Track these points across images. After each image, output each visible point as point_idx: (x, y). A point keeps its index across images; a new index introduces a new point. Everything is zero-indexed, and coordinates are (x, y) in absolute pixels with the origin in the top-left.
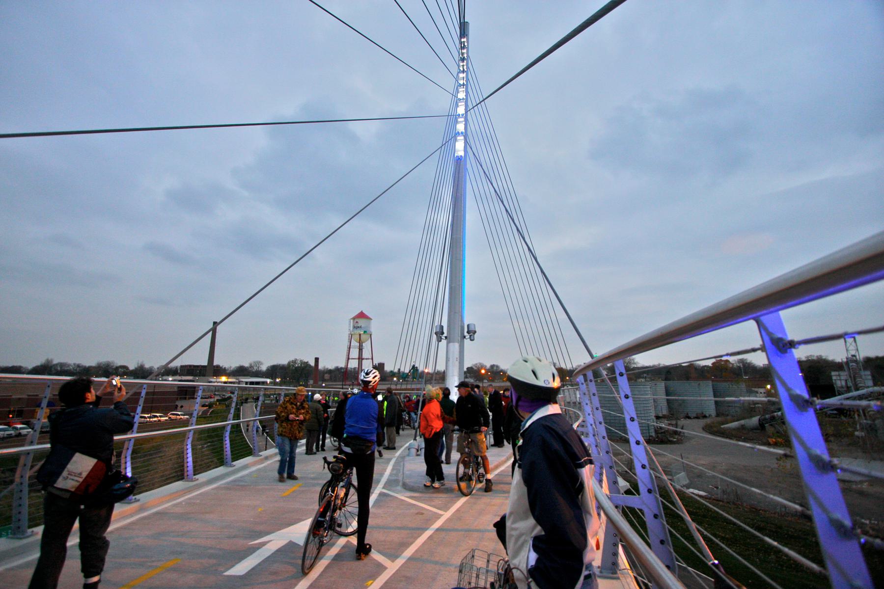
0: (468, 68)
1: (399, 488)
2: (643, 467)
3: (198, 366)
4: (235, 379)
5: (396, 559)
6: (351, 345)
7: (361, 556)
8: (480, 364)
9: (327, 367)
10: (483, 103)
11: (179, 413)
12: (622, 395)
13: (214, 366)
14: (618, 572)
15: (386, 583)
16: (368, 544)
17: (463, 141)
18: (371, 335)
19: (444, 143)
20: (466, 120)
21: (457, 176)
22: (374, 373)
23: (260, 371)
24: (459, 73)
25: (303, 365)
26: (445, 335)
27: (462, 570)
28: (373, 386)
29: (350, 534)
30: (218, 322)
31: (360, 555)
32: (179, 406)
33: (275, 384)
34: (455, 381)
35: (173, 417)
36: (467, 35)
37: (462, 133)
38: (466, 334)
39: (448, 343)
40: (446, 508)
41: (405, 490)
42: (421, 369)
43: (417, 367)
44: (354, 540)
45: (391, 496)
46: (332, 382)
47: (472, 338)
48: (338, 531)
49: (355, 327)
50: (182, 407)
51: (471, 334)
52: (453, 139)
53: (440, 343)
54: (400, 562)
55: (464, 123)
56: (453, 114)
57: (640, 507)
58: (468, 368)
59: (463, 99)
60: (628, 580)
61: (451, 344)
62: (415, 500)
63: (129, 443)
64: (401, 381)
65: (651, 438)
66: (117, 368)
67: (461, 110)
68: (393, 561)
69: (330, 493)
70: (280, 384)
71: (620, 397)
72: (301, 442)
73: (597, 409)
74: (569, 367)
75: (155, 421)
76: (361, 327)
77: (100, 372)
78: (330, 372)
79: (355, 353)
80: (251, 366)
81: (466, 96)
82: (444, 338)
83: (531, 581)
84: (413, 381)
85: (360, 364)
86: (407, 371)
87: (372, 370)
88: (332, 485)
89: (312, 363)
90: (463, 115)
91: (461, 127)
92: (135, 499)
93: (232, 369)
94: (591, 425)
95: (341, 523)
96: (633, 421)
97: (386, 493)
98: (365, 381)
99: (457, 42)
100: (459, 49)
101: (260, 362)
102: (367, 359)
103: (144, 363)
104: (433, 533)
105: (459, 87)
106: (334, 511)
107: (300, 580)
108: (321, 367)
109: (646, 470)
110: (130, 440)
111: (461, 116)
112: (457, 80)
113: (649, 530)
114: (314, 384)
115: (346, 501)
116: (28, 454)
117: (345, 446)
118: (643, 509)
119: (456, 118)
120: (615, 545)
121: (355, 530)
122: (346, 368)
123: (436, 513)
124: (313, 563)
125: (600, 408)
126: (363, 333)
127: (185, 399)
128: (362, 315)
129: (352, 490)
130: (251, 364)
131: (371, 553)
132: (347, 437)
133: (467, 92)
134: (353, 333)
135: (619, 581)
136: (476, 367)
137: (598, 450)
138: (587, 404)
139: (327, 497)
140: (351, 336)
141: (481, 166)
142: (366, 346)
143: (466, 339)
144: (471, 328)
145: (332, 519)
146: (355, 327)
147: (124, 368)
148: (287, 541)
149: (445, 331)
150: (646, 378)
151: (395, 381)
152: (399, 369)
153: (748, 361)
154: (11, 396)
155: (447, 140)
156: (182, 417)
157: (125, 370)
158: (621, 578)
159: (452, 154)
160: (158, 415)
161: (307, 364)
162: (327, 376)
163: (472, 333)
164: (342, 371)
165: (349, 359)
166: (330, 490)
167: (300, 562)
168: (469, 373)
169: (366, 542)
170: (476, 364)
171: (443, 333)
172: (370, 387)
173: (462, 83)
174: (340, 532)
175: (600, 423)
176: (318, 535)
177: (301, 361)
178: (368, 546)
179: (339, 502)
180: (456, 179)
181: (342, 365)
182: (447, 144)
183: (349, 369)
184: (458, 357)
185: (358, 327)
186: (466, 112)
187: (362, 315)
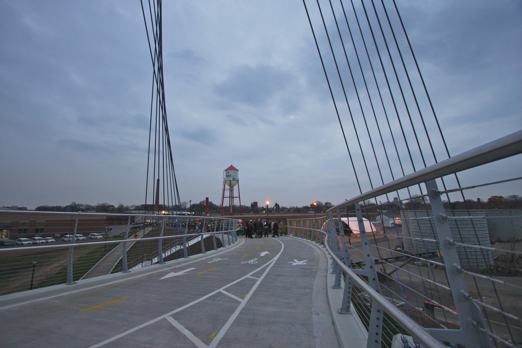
6: (225, 188)
13: (159, 205)
18: (238, 181)
30: (158, 179)
43: (278, 205)
53: (158, 179)
76: (231, 176)
101: (186, 202)
116: (185, 237)
126: (232, 179)
127: (121, 224)
128: (232, 168)
140: (225, 182)
142: (236, 188)
154: (19, 221)
185: (229, 176)
187: (232, 168)
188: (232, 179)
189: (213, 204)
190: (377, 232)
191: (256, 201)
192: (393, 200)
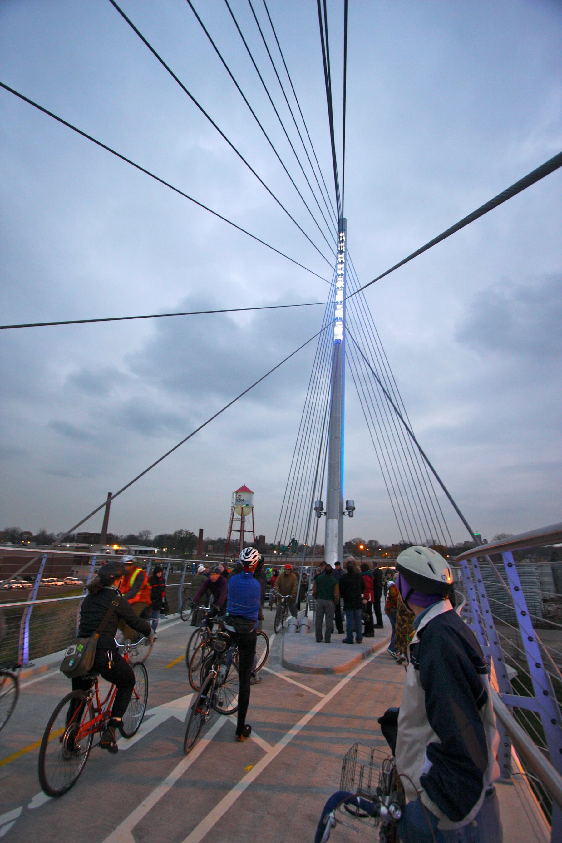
0: (346, 259)
1: (279, 666)
2: (538, 665)
3: (92, 534)
4: (125, 547)
5: (276, 744)
7: (240, 738)
8: (359, 539)
9: (210, 538)
10: (360, 292)
11: (74, 578)
12: (512, 587)
13: (107, 535)
14: (512, 776)
15: (266, 769)
16: (248, 725)
17: (342, 326)
18: (252, 508)
19: (324, 328)
20: (344, 307)
21: (336, 358)
22: (253, 553)
23: (149, 540)
24: (337, 264)
25: (188, 536)
26: (324, 511)
27: (345, 766)
28: (253, 566)
29: (229, 712)
31: (239, 737)
32: (75, 571)
33: (161, 553)
34: (334, 557)
35: (68, 582)
36: (345, 230)
37: (340, 318)
38: (345, 510)
39: (327, 519)
40: (326, 691)
41: (285, 669)
42: (301, 542)
44: (234, 719)
45: (271, 674)
46: (214, 552)
47: (351, 515)
48: (219, 709)
49: (238, 500)
50: (77, 572)
51: (350, 510)
52: (331, 324)
53: (319, 518)
54: (280, 746)
55: (342, 309)
56: (331, 302)
57: (536, 710)
58: (346, 543)
59: (342, 288)
60: (522, 787)
61: (330, 520)
62: (295, 680)
63: (28, 610)
64: (281, 554)
65: (538, 622)
66: (22, 534)
67: (340, 297)
68: (273, 746)
69: (213, 670)
70: (167, 554)
71: (509, 588)
72: (184, 613)
73: (479, 581)
74: (449, 544)
75: (52, 585)
76: (243, 501)
77: (7, 538)
78: (213, 543)
79: (237, 526)
80: (141, 536)
81: (345, 284)
82: (324, 514)
83: (422, 791)
84: (292, 555)
85: (242, 536)
86: (287, 544)
87: (252, 549)
88: (214, 663)
89: (197, 534)
90: (341, 302)
91: (339, 313)
92: (31, 663)
93: (123, 537)
94: (476, 611)
95: (222, 701)
96: (524, 615)
97: (266, 671)
98: (245, 561)
99: (336, 236)
100: (338, 243)
102: (248, 531)
103: (46, 530)
104: (313, 717)
105: (337, 277)
106: (216, 688)
107: (182, 759)
108: (205, 537)
109: (540, 669)
110: (30, 606)
111: (339, 303)
112: (335, 270)
113: (547, 738)
114: (198, 554)
115: (226, 678)
117: (228, 624)
118: (539, 713)
119: (335, 305)
120: (507, 746)
121: (234, 709)
122: (229, 539)
123: (316, 695)
124: (194, 742)
125: (486, 596)
128: (244, 489)
129: (232, 667)
130: (140, 534)
131: (251, 734)
132: (230, 616)
133: (345, 281)
134: (235, 506)
135: (513, 786)
136: (354, 542)
137: (484, 638)
138: (471, 589)
139: (210, 675)
141: (359, 349)
142: (248, 518)
143: (345, 515)
144: (351, 505)
145: (214, 696)
146: (238, 501)
147: (28, 534)
148: (170, 716)
149: (324, 506)
150: (530, 558)
151: (275, 554)
152: (279, 542)
155: (327, 325)
156: (77, 582)
157: (29, 536)
158: (515, 784)
159: (331, 338)
160: (55, 579)
161: (192, 535)
162: (210, 547)
163: (351, 509)
164: (225, 542)
165: (231, 531)
166: (213, 667)
167: (182, 740)
168: (347, 548)
169: (246, 722)
170: (355, 539)
171: (322, 509)
172: (250, 567)
173: (340, 274)
174: (221, 710)
175: (487, 611)
176: (200, 712)
177: (186, 532)
178: (248, 728)
179: (220, 680)
180: (335, 362)
181: (225, 536)
182: (326, 329)
183: (231, 540)
184: (337, 533)
185: (241, 501)
186: (345, 300)
187: (244, 489)
188: (244, 506)
189: (195, 536)
190: (249, 569)
191: (262, 534)
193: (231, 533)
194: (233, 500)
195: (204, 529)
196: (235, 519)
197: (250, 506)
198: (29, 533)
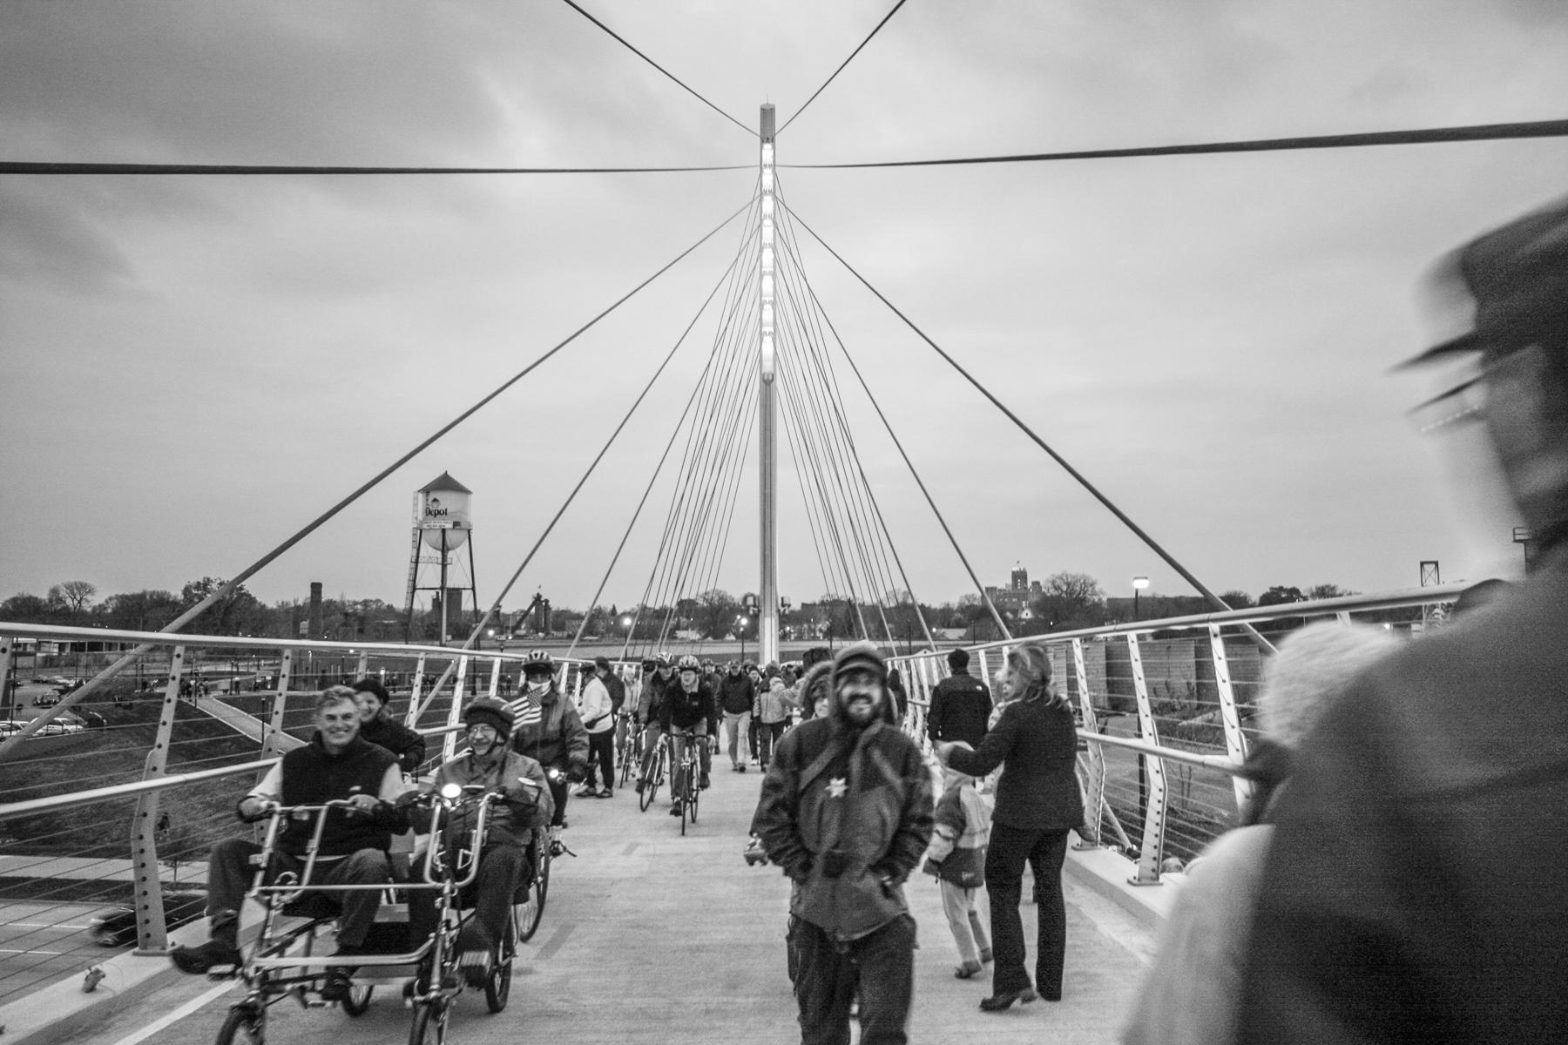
6: (421, 555)
18: (469, 531)
49: (430, 513)
76: (445, 512)
126: (451, 526)
128: (445, 484)
134: (425, 526)
142: (458, 556)
153: (1242, 595)
165: (414, 589)
185: (439, 512)
187: (445, 484)
188: (449, 526)
192: (1010, 582)
193: (415, 595)
194: (417, 511)
195: (323, 584)
196: (423, 560)
197: (463, 525)
198: (390, 607)
